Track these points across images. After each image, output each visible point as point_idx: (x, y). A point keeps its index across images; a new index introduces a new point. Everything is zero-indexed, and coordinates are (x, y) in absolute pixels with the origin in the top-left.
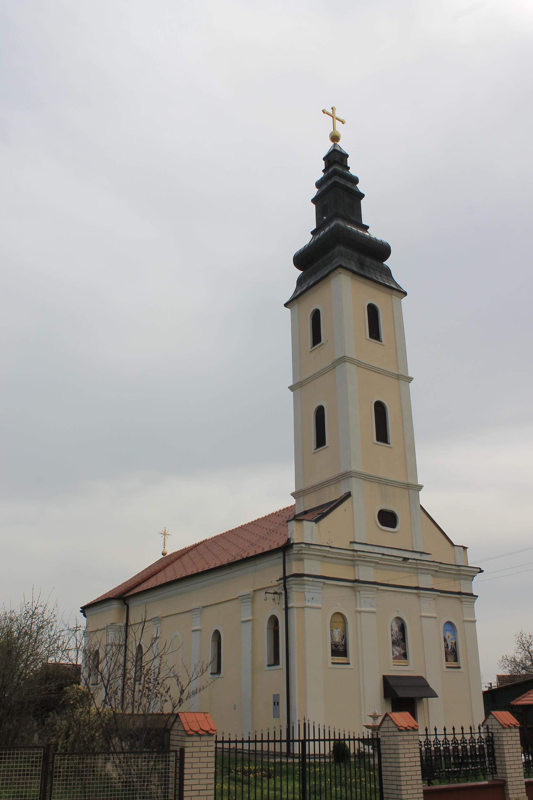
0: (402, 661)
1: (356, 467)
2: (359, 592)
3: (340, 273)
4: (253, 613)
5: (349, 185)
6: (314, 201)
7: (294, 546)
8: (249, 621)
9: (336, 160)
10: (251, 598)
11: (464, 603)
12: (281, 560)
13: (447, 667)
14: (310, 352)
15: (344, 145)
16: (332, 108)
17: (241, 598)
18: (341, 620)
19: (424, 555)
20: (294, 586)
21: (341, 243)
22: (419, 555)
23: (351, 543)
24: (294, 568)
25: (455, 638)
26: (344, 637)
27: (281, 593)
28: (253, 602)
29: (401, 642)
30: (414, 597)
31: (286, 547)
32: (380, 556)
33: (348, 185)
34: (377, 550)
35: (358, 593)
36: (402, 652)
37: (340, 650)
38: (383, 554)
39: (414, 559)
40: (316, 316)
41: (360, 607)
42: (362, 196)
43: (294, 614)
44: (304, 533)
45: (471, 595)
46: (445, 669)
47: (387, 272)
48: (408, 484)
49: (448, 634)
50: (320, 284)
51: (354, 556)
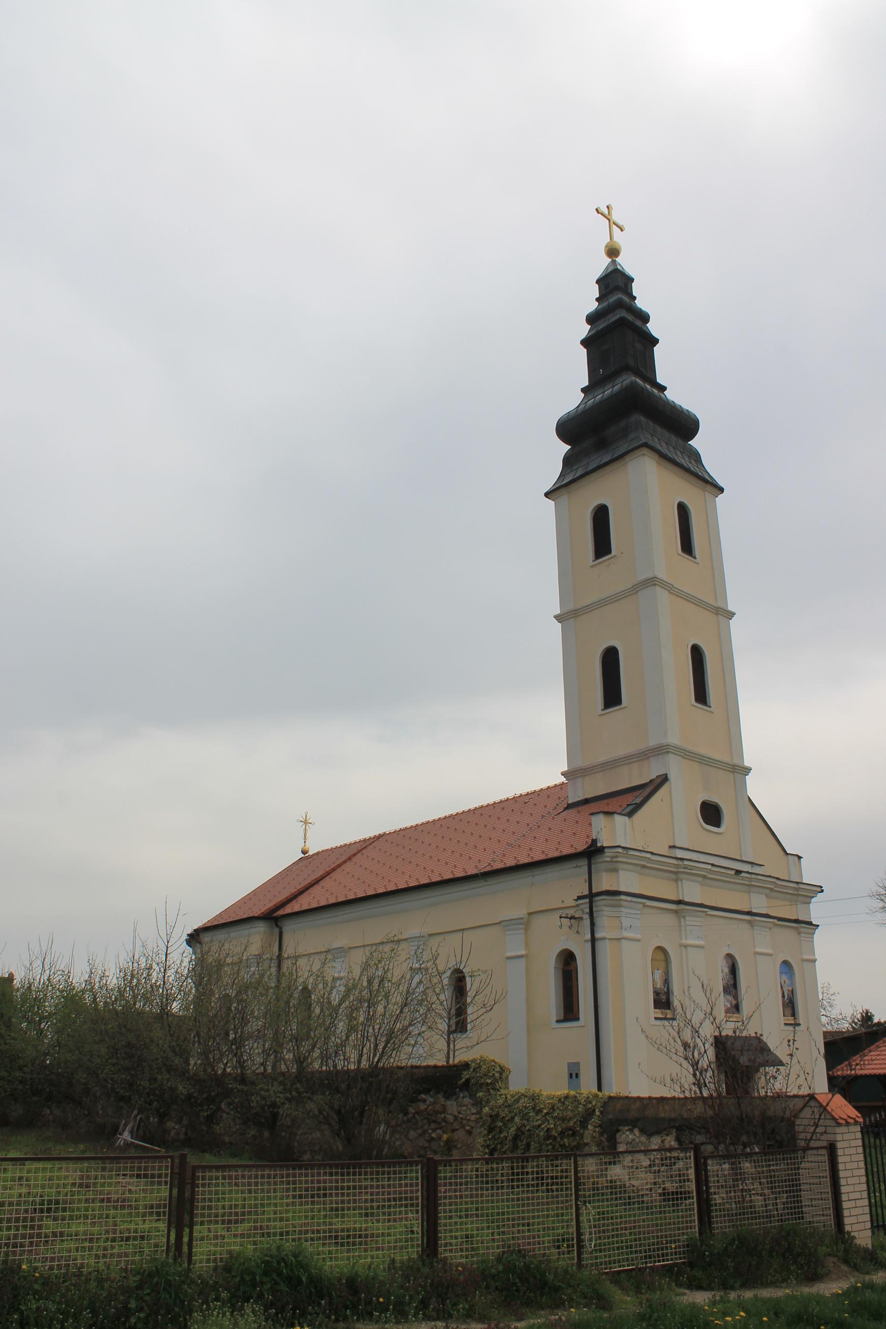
1: (673, 739)
2: (684, 917)
3: (644, 455)
4: (527, 946)
5: (638, 323)
6: (585, 343)
7: (606, 850)
9: (615, 285)
10: (525, 923)
13: (785, 1024)
14: (592, 567)
15: (625, 262)
16: (608, 207)
19: (755, 867)
20: (605, 908)
21: (623, 408)
22: (750, 866)
23: (670, 847)
24: (604, 882)
25: (792, 983)
26: (667, 981)
27: (581, 918)
29: (732, 989)
31: (593, 852)
32: (709, 867)
34: (702, 858)
35: (682, 919)
36: (734, 1002)
37: (663, 1001)
38: (713, 865)
39: (748, 872)
40: (601, 517)
41: (686, 939)
42: (655, 341)
43: (605, 950)
44: (613, 831)
45: (810, 923)
47: (695, 456)
48: (734, 766)
49: (784, 977)
50: (608, 468)
51: (678, 866)
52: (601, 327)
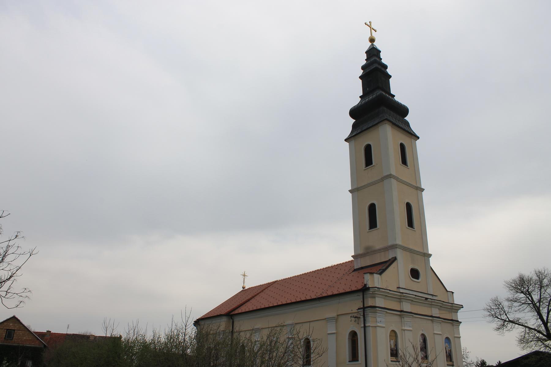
1: (399, 242)
4: (336, 329)
5: (383, 69)
6: (361, 77)
8: (334, 333)
9: (373, 54)
10: (336, 319)
12: (362, 296)
15: (377, 44)
17: (327, 320)
18: (394, 335)
21: (377, 105)
24: (370, 302)
26: (396, 345)
28: (336, 322)
30: (430, 322)
34: (411, 292)
37: (394, 353)
42: (390, 77)
43: (370, 331)
44: (374, 281)
45: (458, 321)
47: (407, 124)
49: (447, 344)
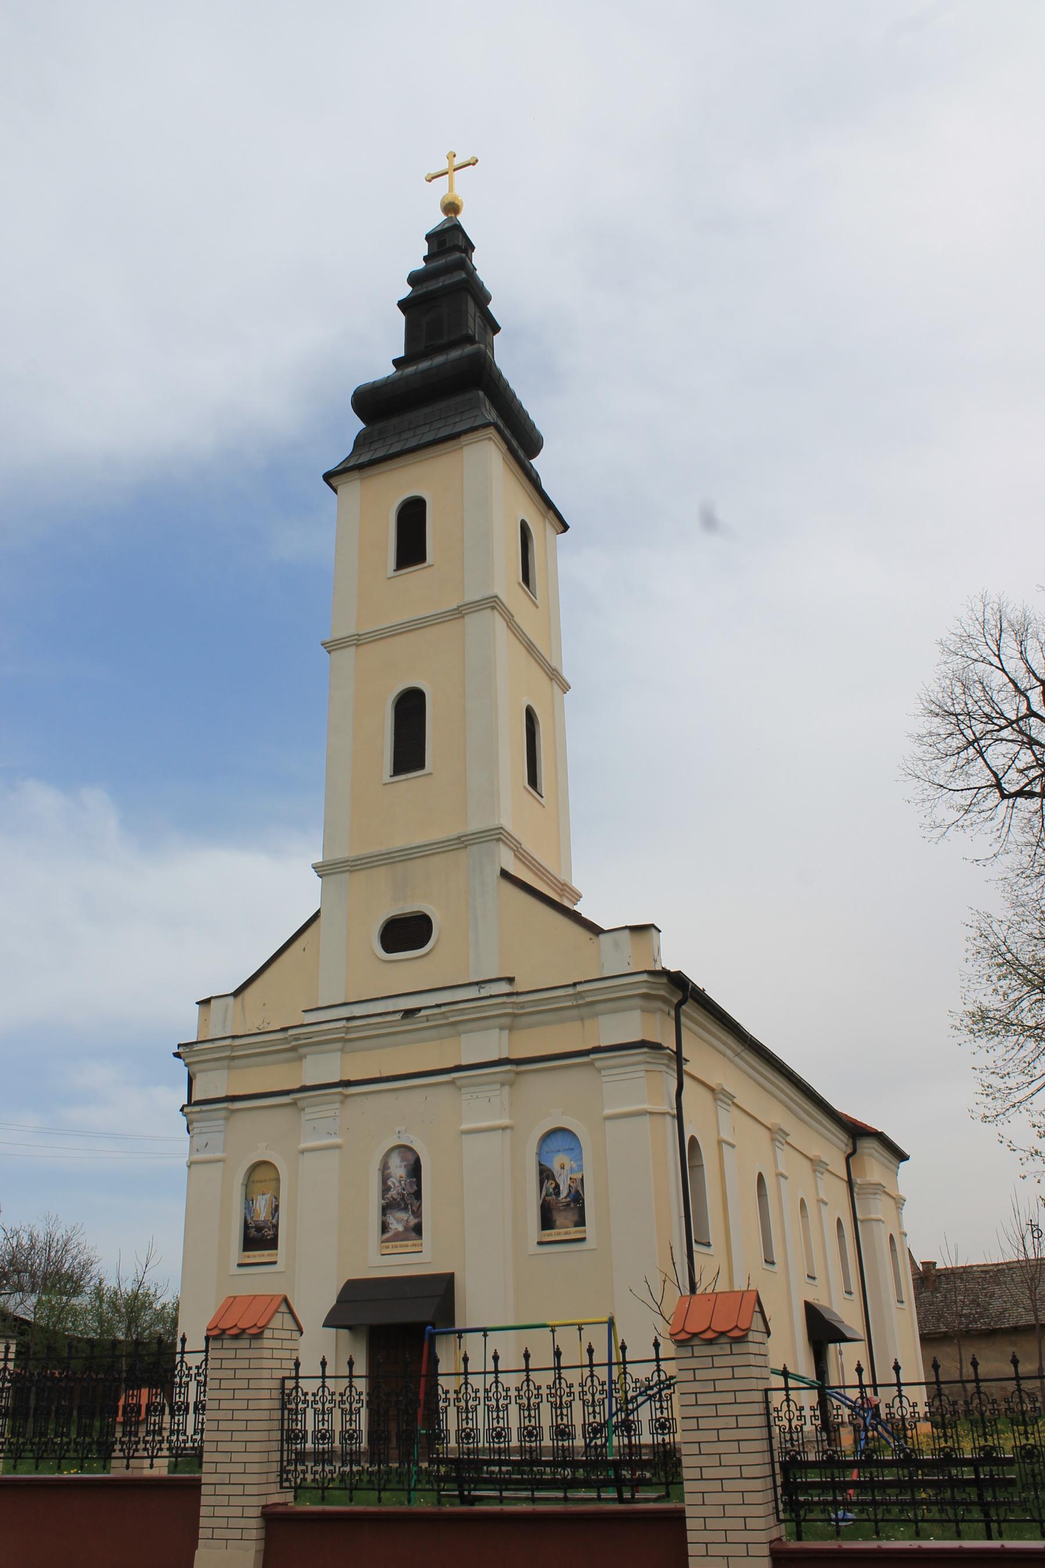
0: (410, 1243)
3: (490, 439)
6: (403, 305)
9: (449, 244)
11: (603, 1073)
19: (487, 986)
22: (476, 988)
25: (581, 1168)
32: (343, 1023)
33: (430, 288)
36: (413, 1221)
38: (348, 1019)
46: (533, 1248)
48: (459, 838)
51: (352, 1027)
52: (421, 292)
